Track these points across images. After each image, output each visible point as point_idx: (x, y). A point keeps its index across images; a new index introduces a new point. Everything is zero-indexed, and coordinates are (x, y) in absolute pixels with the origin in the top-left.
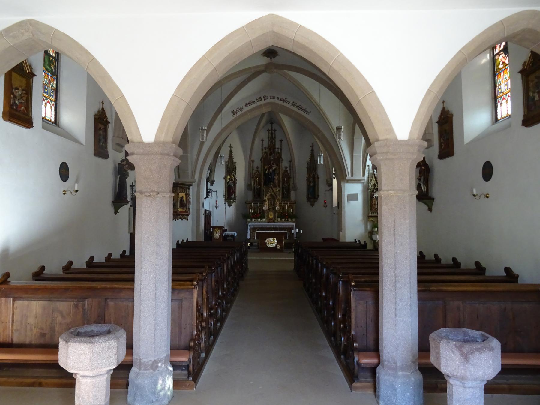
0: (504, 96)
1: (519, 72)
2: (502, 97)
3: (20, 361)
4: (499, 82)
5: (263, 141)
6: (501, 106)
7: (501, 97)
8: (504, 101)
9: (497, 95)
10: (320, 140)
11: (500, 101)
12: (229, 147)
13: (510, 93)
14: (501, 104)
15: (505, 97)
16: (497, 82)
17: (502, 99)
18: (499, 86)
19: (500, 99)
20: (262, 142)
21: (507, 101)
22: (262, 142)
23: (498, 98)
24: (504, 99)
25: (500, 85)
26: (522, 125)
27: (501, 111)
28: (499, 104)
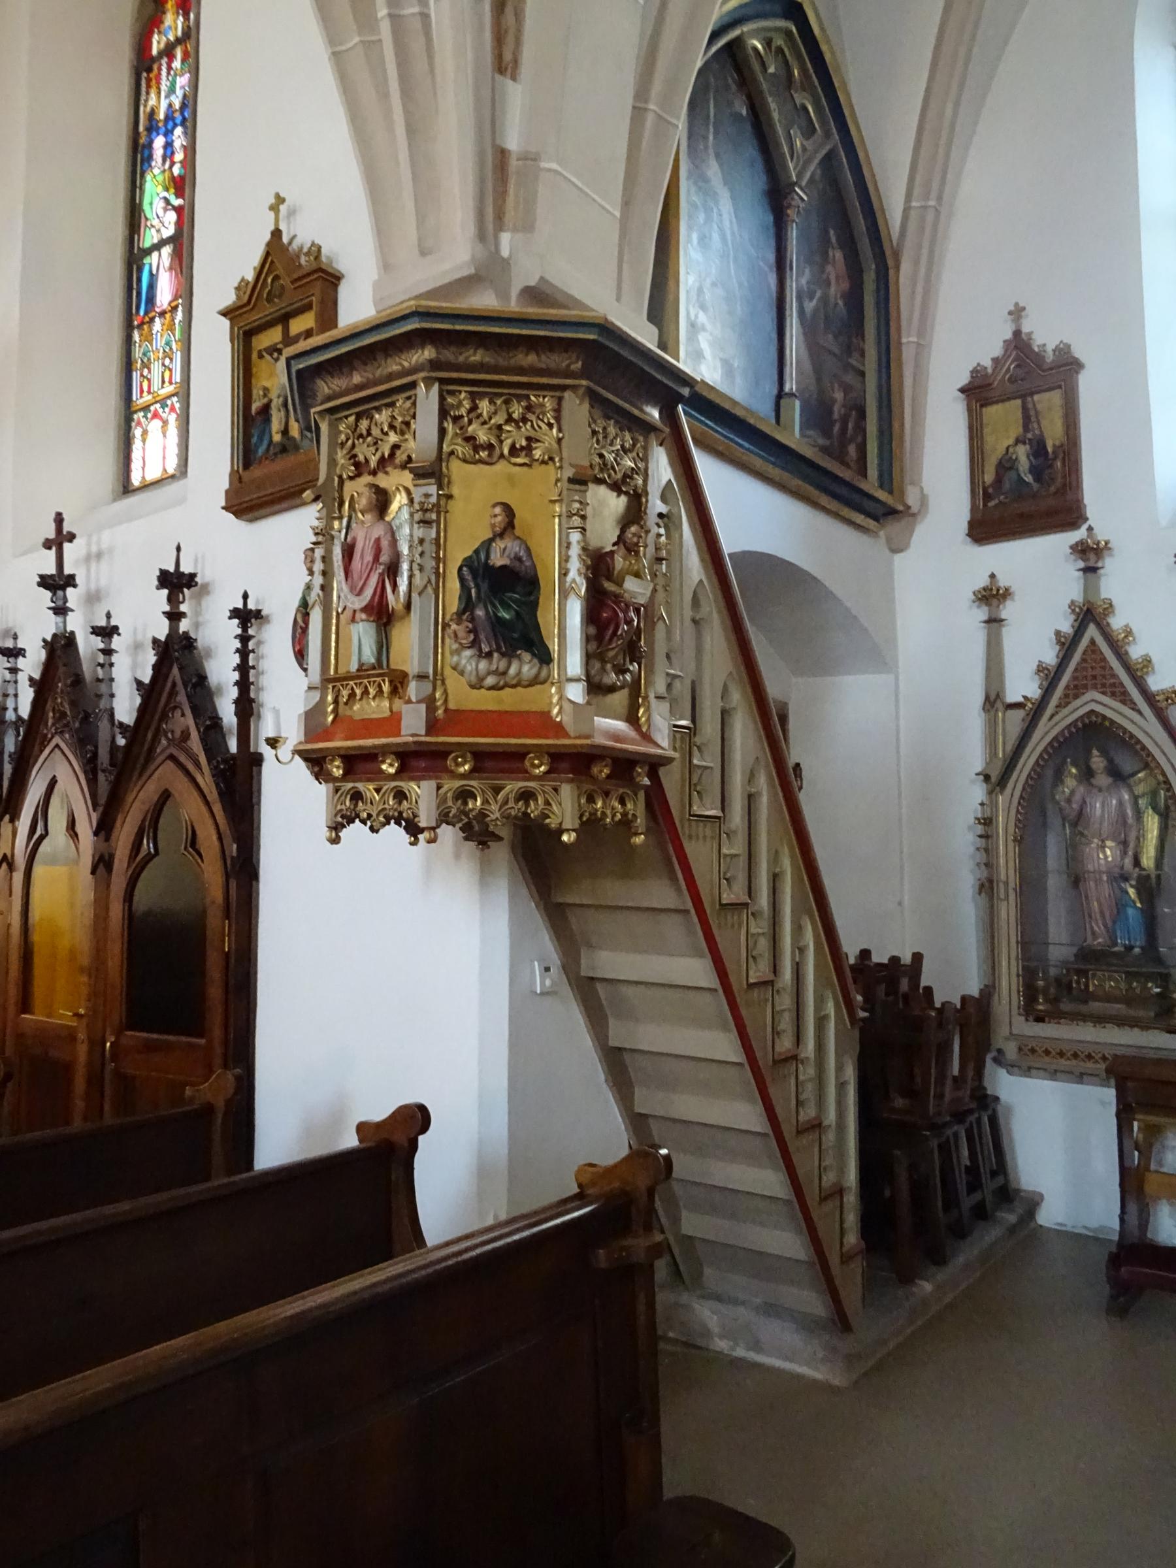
0: (158, 406)
1: (224, 314)
2: (152, 408)
3: (1165, 1053)
4: (144, 354)
5: (1007, 611)
6: (144, 441)
7: (146, 408)
8: (156, 424)
9: (134, 399)
10: (398, 430)
11: (143, 420)
12: (1017, 304)
13: (175, 399)
14: (145, 433)
15: (160, 411)
16: (137, 353)
17: (149, 415)
18: (142, 370)
19: (141, 414)
20: (994, 622)
21: (165, 423)
22: (994, 622)
23: (136, 412)
24: (156, 415)
25: (146, 365)
26: (223, 508)
27: (143, 459)
28: (138, 432)
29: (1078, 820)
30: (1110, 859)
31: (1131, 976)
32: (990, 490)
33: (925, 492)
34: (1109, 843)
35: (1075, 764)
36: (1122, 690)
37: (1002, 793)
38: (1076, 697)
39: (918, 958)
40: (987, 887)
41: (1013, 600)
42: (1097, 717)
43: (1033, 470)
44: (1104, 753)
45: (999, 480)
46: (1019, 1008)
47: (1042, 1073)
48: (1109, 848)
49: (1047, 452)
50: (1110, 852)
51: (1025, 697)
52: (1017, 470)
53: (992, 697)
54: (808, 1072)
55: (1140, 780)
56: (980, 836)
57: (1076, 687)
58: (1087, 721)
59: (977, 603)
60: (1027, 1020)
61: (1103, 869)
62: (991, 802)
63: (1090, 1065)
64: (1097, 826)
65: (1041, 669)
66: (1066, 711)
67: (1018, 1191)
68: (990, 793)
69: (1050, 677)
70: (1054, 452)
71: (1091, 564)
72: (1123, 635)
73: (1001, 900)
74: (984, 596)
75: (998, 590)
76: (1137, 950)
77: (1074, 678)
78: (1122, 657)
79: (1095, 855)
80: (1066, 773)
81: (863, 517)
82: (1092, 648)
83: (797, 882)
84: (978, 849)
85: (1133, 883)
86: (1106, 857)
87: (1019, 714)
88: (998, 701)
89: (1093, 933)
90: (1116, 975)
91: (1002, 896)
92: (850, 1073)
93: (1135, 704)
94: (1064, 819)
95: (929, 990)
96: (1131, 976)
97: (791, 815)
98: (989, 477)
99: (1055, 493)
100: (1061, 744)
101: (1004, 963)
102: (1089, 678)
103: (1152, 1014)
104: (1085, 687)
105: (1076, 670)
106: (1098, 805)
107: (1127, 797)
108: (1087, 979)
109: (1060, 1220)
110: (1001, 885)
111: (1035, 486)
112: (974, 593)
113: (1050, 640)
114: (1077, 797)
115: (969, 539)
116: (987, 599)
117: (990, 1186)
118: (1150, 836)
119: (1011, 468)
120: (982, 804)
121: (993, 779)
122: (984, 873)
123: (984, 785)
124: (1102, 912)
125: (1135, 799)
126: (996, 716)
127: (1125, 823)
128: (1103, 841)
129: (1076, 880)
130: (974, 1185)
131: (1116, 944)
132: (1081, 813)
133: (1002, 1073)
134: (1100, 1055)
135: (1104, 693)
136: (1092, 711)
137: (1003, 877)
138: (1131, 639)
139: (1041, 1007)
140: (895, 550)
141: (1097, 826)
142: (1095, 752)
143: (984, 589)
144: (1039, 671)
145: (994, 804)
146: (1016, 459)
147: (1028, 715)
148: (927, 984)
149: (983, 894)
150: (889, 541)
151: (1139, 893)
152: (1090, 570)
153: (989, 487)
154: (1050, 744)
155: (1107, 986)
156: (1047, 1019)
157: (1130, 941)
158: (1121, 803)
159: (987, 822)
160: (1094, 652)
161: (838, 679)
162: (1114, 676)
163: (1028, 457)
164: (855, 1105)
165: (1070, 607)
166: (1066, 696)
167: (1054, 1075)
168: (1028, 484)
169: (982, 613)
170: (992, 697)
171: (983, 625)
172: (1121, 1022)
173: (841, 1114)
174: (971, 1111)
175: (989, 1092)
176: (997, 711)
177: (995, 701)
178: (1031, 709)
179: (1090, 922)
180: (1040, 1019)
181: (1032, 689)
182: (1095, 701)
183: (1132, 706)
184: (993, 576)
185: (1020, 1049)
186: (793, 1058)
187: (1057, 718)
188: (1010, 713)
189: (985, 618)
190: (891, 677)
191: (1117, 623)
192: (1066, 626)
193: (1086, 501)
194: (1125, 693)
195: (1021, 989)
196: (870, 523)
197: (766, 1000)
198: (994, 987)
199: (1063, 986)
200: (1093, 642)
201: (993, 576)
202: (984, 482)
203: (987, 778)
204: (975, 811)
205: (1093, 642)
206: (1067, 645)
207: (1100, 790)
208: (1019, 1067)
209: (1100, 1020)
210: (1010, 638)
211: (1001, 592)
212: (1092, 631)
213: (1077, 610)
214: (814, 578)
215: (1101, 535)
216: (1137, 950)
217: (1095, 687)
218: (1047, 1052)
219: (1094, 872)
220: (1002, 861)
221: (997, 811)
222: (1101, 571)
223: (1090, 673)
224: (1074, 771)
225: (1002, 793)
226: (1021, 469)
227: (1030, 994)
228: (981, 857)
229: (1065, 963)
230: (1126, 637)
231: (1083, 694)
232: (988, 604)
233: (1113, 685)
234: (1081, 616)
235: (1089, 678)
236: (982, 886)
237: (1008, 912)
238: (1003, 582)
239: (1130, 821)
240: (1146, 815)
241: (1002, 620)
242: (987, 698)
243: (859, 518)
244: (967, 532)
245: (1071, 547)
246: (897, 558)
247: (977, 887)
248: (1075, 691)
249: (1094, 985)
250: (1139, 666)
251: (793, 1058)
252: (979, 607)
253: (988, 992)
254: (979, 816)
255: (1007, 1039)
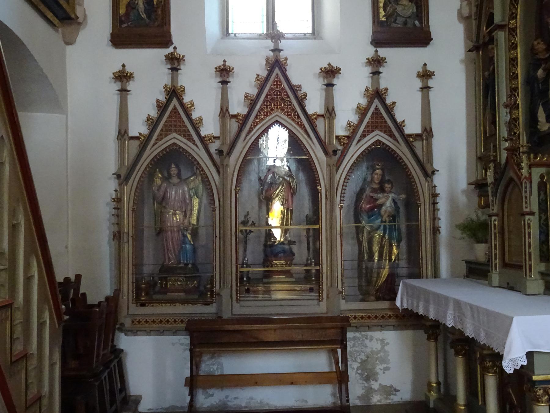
5: (131, 86)
20: (124, 91)
22: (124, 91)
29: (163, 201)
30: (178, 220)
31: (188, 278)
32: (123, 18)
33: (86, 13)
34: (178, 212)
35: (160, 172)
36: (188, 133)
37: (126, 186)
38: (166, 136)
39: (78, 277)
40: (117, 236)
41: (134, 81)
42: (176, 146)
43: (146, 11)
44: (177, 166)
45: (127, 14)
46: (133, 300)
47: (141, 333)
48: (178, 214)
49: (154, 4)
50: (178, 217)
51: (140, 134)
52: (138, 10)
53: (123, 132)
54: (33, 362)
55: (192, 181)
56: (114, 208)
57: (166, 130)
58: (165, 152)
59: (114, 80)
60: (137, 306)
61: (175, 225)
62: (121, 189)
63: (169, 325)
64: (172, 203)
65: (149, 119)
66: (160, 143)
67: (130, 396)
68: (120, 184)
69: (152, 123)
70: (157, 4)
71: (175, 66)
72: (190, 105)
73: (126, 243)
74: (119, 76)
75: (127, 74)
76: (190, 266)
77: (165, 125)
78: (189, 116)
79: (171, 219)
80: (156, 176)
81: (52, 14)
82: (175, 111)
83: (28, 229)
84: (113, 215)
85: (189, 232)
86: (177, 219)
87: (136, 143)
88: (126, 135)
89: (169, 258)
90: (181, 279)
91: (125, 240)
92: (57, 357)
93: (194, 141)
94: (154, 199)
95: (84, 295)
96: (188, 278)
97: (25, 183)
98: (122, 11)
99: (158, 26)
100: (158, 160)
101: (125, 277)
102: (173, 126)
103: (198, 297)
104: (171, 130)
105: (166, 121)
106: (173, 193)
107: (186, 189)
108: (166, 281)
109: (149, 407)
110: (125, 235)
111: (147, 21)
112: (114, 74)
113: (153, 104)
114: (163, 189)
115: (110, 43)
116: (121, 78)
117: (119, 397)
118: (194, 209)
119: (133, 8)
120: (116, 191)
121: (122, 178)
122: (116, 228)
123: (117, 181)
124: (174, 249)
125: (189, 189)
126: (124, 144)
127: (185, 202)
128: (175, 211)
129: (160, 232)
130: (113, 402)
131: (180, 263)
132: (164, 198)
133: (122, 335)
134: (173, 320)
135: (180, 135)
136: (174, 143)
137: (126, 231)
138: (193, 108)
139: (143, 299)
140: (68, 43)
141: (172, 203)
142: (173, 166)
143: (120, 71)
144: (148, 120)
145: (122, 190)
146: (137, 4)
147: (142, 143)
148: (83, 292)
149: (115, 240)
150: (64, 37)
151: (192, 237)
152: (175, 70)
153: (122, 16)
154: (153, 159)
155: (176, 285)
156: (147, 305)
157: (187, 261)
158: (183, 191)
159: (118, 200)
160: (175, 113)
161: (29, 114)
162: (185, 126)
163: (143, 3)
164: (59, 377)
165: (164, 88)
166: (161, 135)
167: (148, 333)
168: (143, 19)
169: (117, 86)
170: (123, 132)
171: (117, 92)
172: (184, 302)
173: (51, 385)
174: (111, 361)
175: (117, 347)
176: (125, 140)
177: (124, 134)
178: (143, 140)
179: (168, 253)
180: (143, 305)
181: (144, 130)
182: (175, 138)
183: (193, 142)
184: (124, 66)
185: (133, 322)
186: (25, 357)
187: (156, 146)
188: (131, 141)
189: (120, 88)
190: (65, 116)
191: (186, 99)
192: (162, 98)
193: (173, 33)
194: (190, 135)
195: (134, 290)
196: (56, 21)
197: (6, 319)
198: (120, 290)
199: (151, 285)
200: (175, 108)
201: (124, 66)
202: (119, 13)
203: (118, 176)
204: (111, 195)
205: (175, 108)
206: (162, 108)
207: (174, 185)
208: (131, 331)
209: (172, 302)
210: (131, 100)
211: (129, 75)
212: (175, 102)
213: (168, 89)
214: (23, 44)
215: (180, 51)
216: (190, 266)
217: (175, 131)
218: (146, 322)
219: (171, 227)
220: (126, 222)
221: (124, 194)
222: (180, 72)
223: (173, 123)
224: (160, 175)
225: (126, 184)
226: (140, 10)
227: (138, 291)
228: (114, 220)
229: (152, 275)
230: (191, 107)
231: (170, 134)
232: (121, 81)
233: (184, 131)
234: (170, 93)
235: (173, 126)
236: (114, 236)
237: (128, 249)
238: (128, 69)
239: (188, 201)
240: (193, 198)
241: (129, 91)
242: (120, 132)
243: (50, 15)
244: (110, 39)
245: (166, 56)
246: (69, 48)
247: (112, 237)
248: (165, 132)
249: (170, 284)
250: (197, 122)
251: (25, 357)
252: (115, 82)
253: (117, 292)
254: (114, 197)
255: (126, 317)
